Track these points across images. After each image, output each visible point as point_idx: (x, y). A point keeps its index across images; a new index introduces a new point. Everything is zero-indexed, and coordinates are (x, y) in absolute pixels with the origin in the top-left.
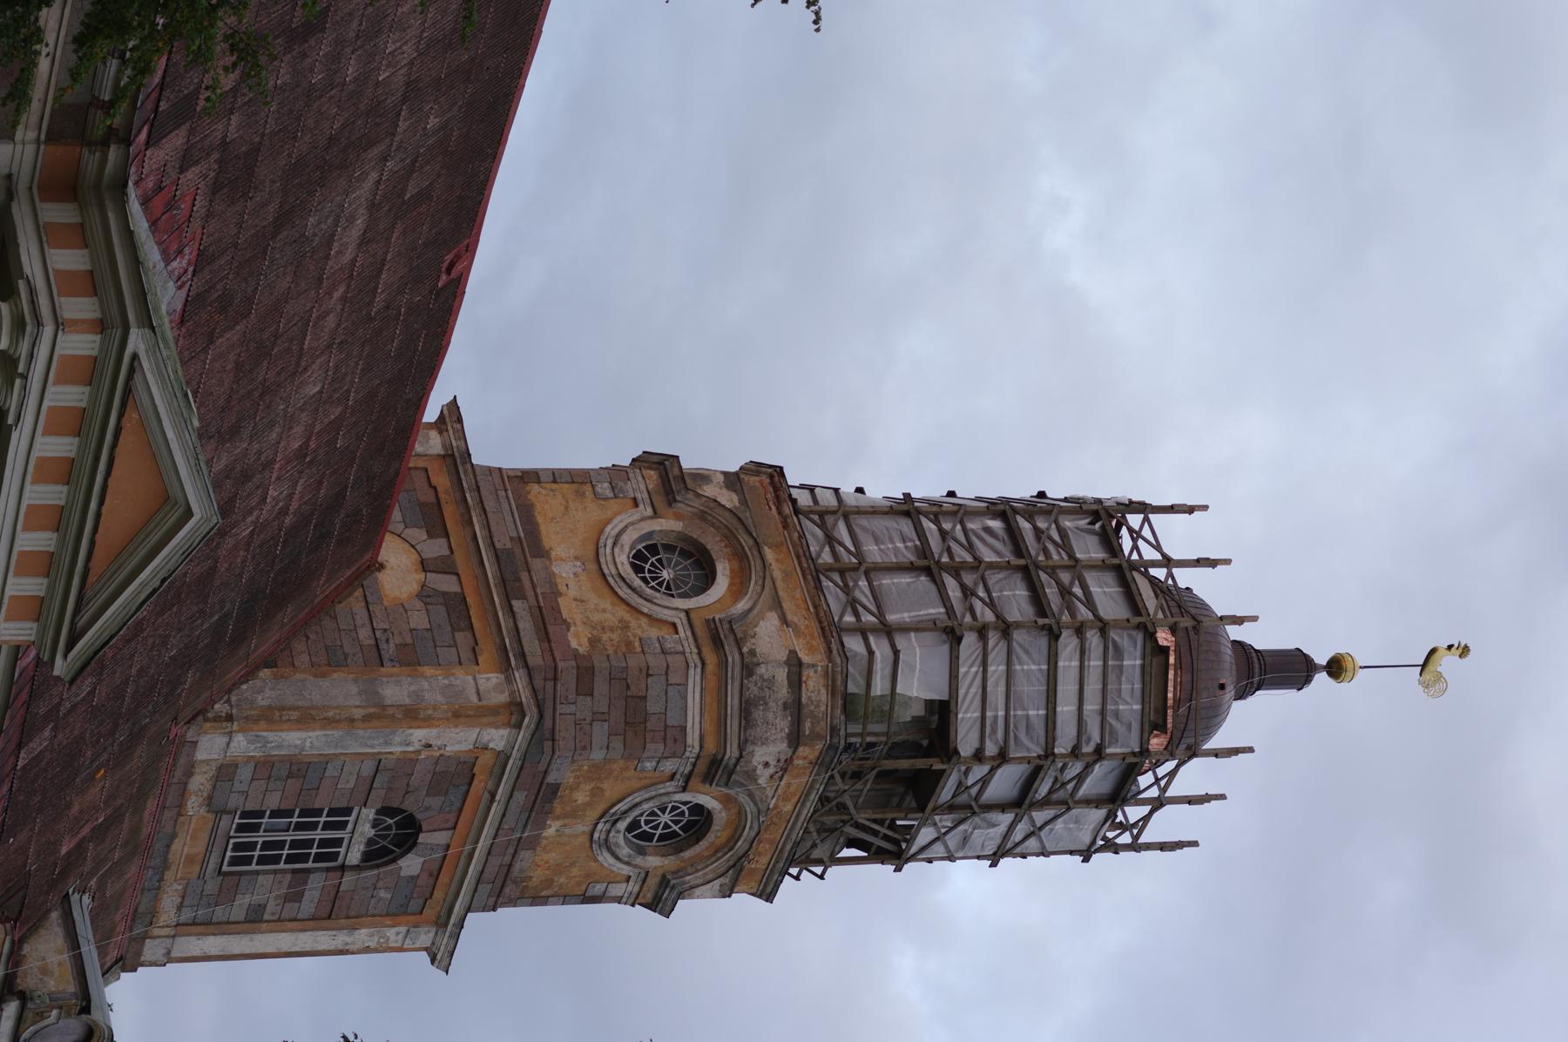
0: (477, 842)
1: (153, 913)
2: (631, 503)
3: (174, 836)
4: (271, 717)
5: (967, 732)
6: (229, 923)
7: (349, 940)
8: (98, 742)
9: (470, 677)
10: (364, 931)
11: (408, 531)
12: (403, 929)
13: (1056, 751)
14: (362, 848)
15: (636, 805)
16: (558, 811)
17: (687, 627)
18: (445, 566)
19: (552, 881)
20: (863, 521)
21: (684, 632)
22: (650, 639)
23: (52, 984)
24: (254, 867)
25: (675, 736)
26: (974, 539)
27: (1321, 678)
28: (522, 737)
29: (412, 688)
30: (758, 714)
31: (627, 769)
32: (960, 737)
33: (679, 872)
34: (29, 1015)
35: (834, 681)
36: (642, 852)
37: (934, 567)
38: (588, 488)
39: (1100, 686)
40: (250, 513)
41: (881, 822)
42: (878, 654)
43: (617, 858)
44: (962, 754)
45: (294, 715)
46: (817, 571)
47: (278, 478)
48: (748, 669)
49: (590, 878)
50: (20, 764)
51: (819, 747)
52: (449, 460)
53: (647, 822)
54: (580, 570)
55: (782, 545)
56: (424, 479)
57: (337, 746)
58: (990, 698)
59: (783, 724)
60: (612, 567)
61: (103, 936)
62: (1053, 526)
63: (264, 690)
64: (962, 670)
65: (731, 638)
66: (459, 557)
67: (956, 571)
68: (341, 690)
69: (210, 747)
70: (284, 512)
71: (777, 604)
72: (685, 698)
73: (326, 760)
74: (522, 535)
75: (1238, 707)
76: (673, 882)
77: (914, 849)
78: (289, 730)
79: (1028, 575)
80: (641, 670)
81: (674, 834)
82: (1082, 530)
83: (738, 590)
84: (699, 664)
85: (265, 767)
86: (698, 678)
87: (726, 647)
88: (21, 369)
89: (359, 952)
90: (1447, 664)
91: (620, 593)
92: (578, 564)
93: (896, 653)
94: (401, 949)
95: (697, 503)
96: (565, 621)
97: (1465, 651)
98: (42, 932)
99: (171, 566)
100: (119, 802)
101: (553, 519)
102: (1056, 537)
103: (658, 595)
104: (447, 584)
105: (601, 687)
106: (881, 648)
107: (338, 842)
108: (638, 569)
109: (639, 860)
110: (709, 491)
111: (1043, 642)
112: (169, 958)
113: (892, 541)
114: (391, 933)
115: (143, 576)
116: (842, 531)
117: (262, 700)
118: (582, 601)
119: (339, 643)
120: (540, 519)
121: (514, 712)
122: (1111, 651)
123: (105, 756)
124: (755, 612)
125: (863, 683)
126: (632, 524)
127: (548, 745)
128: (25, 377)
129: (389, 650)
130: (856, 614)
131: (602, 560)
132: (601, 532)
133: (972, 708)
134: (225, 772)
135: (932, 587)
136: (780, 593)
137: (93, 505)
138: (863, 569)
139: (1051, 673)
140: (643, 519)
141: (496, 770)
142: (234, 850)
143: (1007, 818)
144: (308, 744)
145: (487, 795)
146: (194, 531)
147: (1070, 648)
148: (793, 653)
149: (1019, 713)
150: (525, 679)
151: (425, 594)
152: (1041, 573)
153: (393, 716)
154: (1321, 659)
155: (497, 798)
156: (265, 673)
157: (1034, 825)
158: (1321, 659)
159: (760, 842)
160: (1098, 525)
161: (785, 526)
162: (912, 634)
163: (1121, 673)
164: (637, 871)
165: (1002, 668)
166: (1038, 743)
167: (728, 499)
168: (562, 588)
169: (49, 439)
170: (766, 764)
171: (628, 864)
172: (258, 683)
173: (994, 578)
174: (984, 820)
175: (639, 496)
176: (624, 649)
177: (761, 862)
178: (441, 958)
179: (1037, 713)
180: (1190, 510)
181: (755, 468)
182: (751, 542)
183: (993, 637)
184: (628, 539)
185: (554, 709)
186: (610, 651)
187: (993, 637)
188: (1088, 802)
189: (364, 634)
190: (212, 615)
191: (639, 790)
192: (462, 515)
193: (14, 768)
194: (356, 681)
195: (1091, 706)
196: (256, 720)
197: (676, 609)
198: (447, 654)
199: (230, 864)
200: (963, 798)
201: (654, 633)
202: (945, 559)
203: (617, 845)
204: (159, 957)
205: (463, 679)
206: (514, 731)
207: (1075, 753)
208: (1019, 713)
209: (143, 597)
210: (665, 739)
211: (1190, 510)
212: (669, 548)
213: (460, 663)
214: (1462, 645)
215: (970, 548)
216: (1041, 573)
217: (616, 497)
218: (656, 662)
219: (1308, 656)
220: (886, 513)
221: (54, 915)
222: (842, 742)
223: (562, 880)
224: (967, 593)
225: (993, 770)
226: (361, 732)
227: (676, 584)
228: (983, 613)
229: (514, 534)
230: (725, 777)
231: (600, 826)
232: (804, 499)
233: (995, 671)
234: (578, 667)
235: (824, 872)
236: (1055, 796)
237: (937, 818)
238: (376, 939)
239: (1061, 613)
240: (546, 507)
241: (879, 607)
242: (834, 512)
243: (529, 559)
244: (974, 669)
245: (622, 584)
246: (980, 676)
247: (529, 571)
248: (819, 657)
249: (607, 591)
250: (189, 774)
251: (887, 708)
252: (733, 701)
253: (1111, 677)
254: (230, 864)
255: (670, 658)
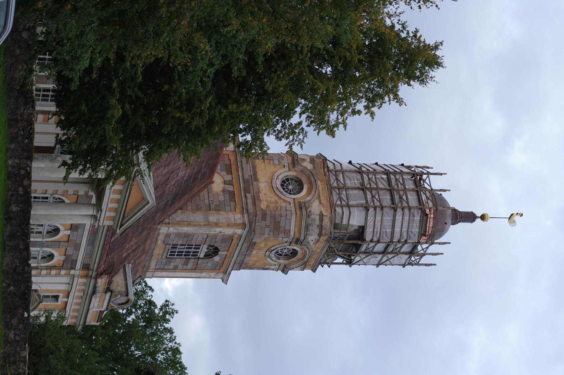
0: (232, 258)
1: (149, 266)
2: (283, 166)
3: (154, 249)
4: (179, 223)
5: (369, 234)
6: (169, 269)
7: (200, 275)
8: (133, 232)
9: (233, 215)
10: (204, 273)
11: (222, 172)
12: (215, 273)
13: (394, 241)
14: (204, 254)
15: (277, 248)
16: (256, 248)
17: (293, 203)
18: (230, 183)
19: (255, 264)
20: (347, 174)
21: (292, 205)
22: (283, 206)
23: (119, 289)
24: (175, 257)
25: (287, 233)
26: (378, 180)
27: (478, 220)
28: (245, 232)
29: (217, 217)
30: (310, 228)
31: (274, 239)
32: (367, 236)
33: (289, 264)
34: (113, 296)
35: (332, 220)
36: (279, 259)
37: (364, 189)
38: (272, 161)
39: (407, 224)
40: (174, 179)
41: (345, 255)
42: (345, 213)
43: (272, 260)
44: (367, 240)
45: (186, 223)
46: (331, 188)
47: (182, 171)
48: (308, 216)
49: (266, 264)
50: (112, 241)
51: (327, 237)
52: (235, 152)
53: (280, 252)
54: (267, 186)
55: (323, 180)
56: (228, 158)
57: (197, 231)
58: (376, 225)
59: (317, 231)
60: (275, 185)
61: (134, 274)
62: (401, 177)
63: (179, 216)
64: (369, 218)
65: (304, 208)
66: (234, 180)
67: (371, 189)
68: (199, 217)
69: (164, 230)
70: (184, 177)
71: (319, 198)
72: (291, 223)
73: (194, 234)
74: (252, 175)
75: (452, 227)
76: (287, 267)
77: (354, 262)
78: (184, 227)
79: (391, 191)
80: (279, 215)
81: (288, 255)
82: (409, 179)
83: (309, 193)
84: (295, 214)
85: (178, 235)
86: (295, 217)
87: (303, 210)
88: (98, 219)
89: (203, 278)
90: (517, 218)
91: (276, 193)
92: (266, 183)
93: (350, 213)
94: (214, 278)
95: (301, 168)
96: (260, 200)
97: (522, 215)
98: (118, 274)
99: (144, 213)
100: (139, 244)
101: (261, 170)
102: (401, 182)
103: (286, 194)
104: (230, 188)
105: (268, 219)
106: (346, 211)
107: (198, 252)
108: (282, 185)
109: (278, 261)
110: (305, 164)
111: (392, 211)
112: (153, 277)
113: (354, 181)
114: (212, 274)
115: (138, 214)
116: (341, 178)
117: (178, 219)
118: (266, 194)
119: (200, 204)
120: (257, 170)
121: (244, 225)
122: (411, 215)
123: (135, 235)
124: (313, 200)
125: (340, 221)
126: (282, 173)
127: (253, 233)
128: (99, 220)
129: (213, 206)
130: (341, 202)
131: (273, 183)
132: (274, 175)
133: (371, 228)
134: (168, 235)
135: (363, 194)
136: (321, 194)
137: (126, 200)
138: (344, 188)
139: (394, 220)
140: (286, 171)
141: (239, 238)
142: (170, 253)
143: (380, 256)
144: (189, 230)
145: (236, 244)
146: (150, 206)
147: (400, 213)
148: (321, 212)
149: (384, 230)
150: (247, 216)
151: (224, 191)
152: (395, 192)
153: (211, 225)
154: (479, 214)
155: (239, 245)
156: (179, 211)
157: (388, 258)
158: (479, 214)
159: (311, 258)
160: (413, 178)
161: (325, 175)
162: (356, 208)
163: (414, 221)
164: (277, 263)
165: (380, 218)
166: (389, 238)
167: (310, 166)
168: (261, 190)
169: (113, 195)
170: (312, 240)
171: (275, 261)
172: (177, 214)
173: (381, 192)
174: (374, 256)
175: (285, 164)
176: (275, 209)
177: (312, 262)
178: (225, 281)
179: (389, 230)
180: (441, 174)
181: (320, 156)
182: (314, 180)
183: (378, 210)
184: (280, 177)
185: (255, 224)
186: (272, 209)
187: (378, 210)
188: (403, 253)
189: (207, 202)
190: (164, 201)
191: (278, 244)
192: (236, 168)
193: (110, 241)
194: (203, 214)
195: (405, 229)
196: (176, 224)
197: (291, 198)
198: (228, 208)
199: (169, 256)
200: (368, 251)
201: (284, 204)
202: (368, 186)
203: (272, 257)
204: (151, 275)
205: (231, 215)
206: (243, 230)
207: (399, 241)
208: (384, 230)
209: (138, 219)
210: (284, 233)
211: (441, 174)
212: (292, 179)
213: (231, 211)
214: (521, 213)
215: (376, 184)
216: (395, 192)
217: (279, 165)
218: (283, 213)
219: (475, 214)
220: (354, 172)
221: (121, 270)
222: (333, 236)
223: (257, 264)
224: (373, 197)
225: (376, 244)
226: (203, 228)
227: (293, 190)
228: (376, 203)
229: (250, 174)
230: (300, 243)
231: (267, 252)
232: (331, 166)
233: (378, 219)
234: (262, 213)
235: (330, 265)
236: (394, 251)
237: (361, 255)
238: (208, 275)
239: (398, 204)
240: (260, 166)
241: (347, 200)
242: (339, 171)
243: (253, 182)
244: (372, 218)
245: (277, 190)
246: (374, 219)
247: (253, 185)
248: (328, 213)
249: (273, 192)
250: (158, 235)
251: (347, 227)
252: (303, 224)
253: (411, 222)
254: (169, 256)
255: (287, 212)
